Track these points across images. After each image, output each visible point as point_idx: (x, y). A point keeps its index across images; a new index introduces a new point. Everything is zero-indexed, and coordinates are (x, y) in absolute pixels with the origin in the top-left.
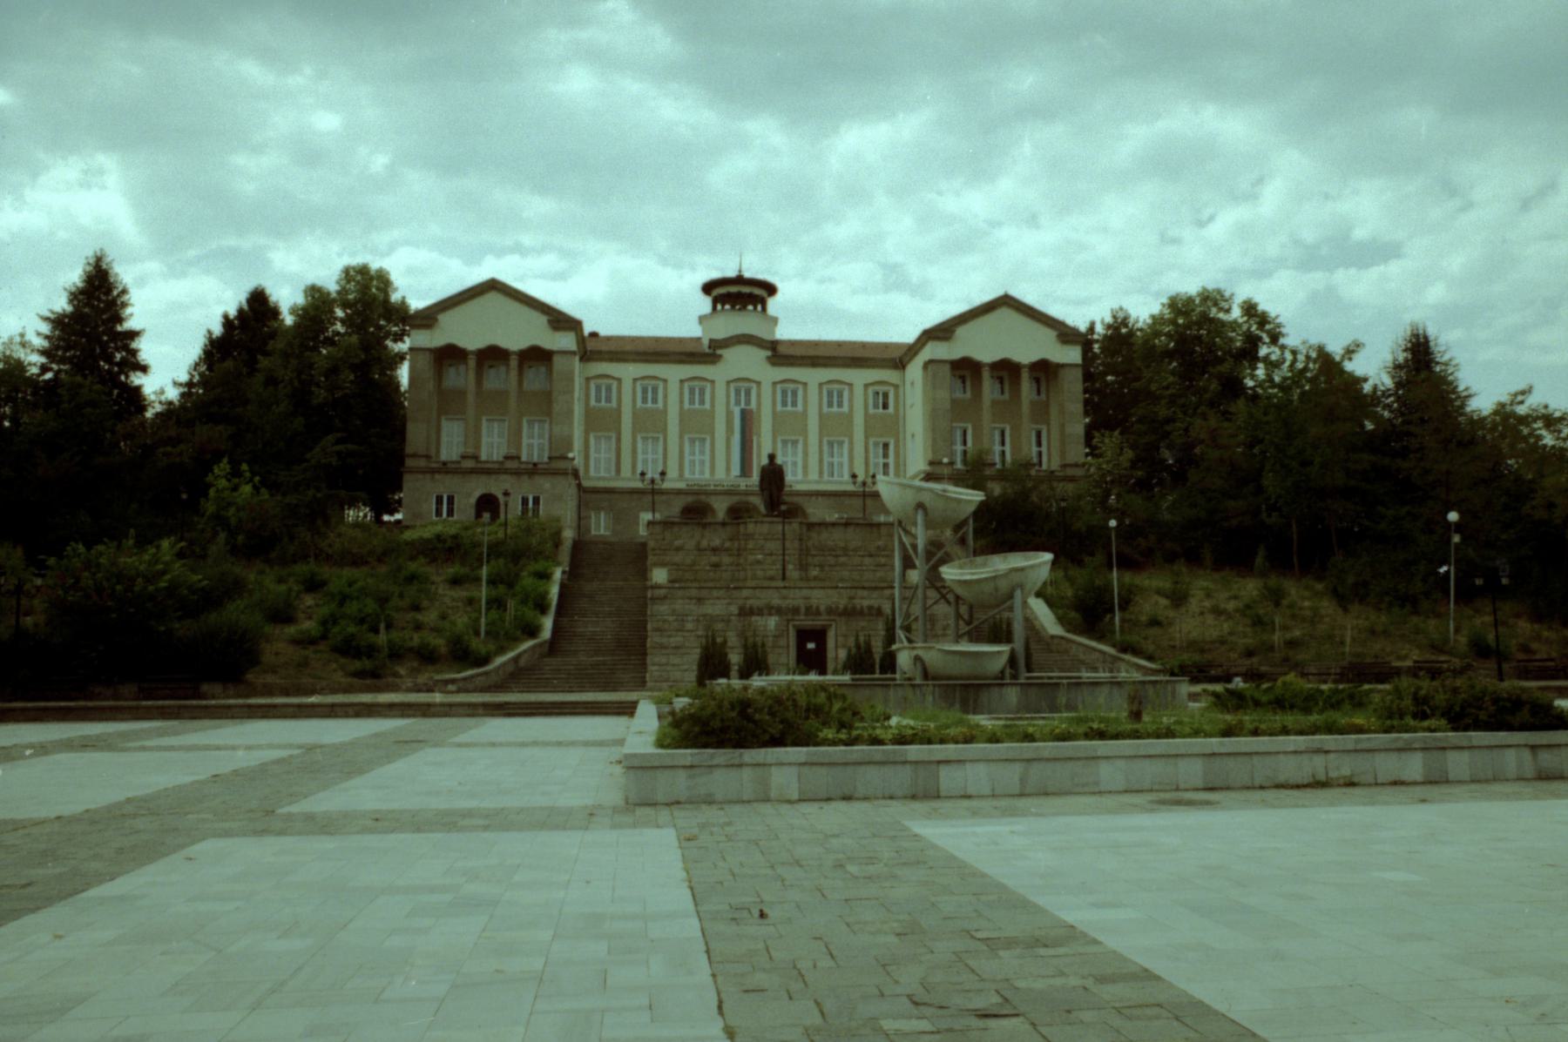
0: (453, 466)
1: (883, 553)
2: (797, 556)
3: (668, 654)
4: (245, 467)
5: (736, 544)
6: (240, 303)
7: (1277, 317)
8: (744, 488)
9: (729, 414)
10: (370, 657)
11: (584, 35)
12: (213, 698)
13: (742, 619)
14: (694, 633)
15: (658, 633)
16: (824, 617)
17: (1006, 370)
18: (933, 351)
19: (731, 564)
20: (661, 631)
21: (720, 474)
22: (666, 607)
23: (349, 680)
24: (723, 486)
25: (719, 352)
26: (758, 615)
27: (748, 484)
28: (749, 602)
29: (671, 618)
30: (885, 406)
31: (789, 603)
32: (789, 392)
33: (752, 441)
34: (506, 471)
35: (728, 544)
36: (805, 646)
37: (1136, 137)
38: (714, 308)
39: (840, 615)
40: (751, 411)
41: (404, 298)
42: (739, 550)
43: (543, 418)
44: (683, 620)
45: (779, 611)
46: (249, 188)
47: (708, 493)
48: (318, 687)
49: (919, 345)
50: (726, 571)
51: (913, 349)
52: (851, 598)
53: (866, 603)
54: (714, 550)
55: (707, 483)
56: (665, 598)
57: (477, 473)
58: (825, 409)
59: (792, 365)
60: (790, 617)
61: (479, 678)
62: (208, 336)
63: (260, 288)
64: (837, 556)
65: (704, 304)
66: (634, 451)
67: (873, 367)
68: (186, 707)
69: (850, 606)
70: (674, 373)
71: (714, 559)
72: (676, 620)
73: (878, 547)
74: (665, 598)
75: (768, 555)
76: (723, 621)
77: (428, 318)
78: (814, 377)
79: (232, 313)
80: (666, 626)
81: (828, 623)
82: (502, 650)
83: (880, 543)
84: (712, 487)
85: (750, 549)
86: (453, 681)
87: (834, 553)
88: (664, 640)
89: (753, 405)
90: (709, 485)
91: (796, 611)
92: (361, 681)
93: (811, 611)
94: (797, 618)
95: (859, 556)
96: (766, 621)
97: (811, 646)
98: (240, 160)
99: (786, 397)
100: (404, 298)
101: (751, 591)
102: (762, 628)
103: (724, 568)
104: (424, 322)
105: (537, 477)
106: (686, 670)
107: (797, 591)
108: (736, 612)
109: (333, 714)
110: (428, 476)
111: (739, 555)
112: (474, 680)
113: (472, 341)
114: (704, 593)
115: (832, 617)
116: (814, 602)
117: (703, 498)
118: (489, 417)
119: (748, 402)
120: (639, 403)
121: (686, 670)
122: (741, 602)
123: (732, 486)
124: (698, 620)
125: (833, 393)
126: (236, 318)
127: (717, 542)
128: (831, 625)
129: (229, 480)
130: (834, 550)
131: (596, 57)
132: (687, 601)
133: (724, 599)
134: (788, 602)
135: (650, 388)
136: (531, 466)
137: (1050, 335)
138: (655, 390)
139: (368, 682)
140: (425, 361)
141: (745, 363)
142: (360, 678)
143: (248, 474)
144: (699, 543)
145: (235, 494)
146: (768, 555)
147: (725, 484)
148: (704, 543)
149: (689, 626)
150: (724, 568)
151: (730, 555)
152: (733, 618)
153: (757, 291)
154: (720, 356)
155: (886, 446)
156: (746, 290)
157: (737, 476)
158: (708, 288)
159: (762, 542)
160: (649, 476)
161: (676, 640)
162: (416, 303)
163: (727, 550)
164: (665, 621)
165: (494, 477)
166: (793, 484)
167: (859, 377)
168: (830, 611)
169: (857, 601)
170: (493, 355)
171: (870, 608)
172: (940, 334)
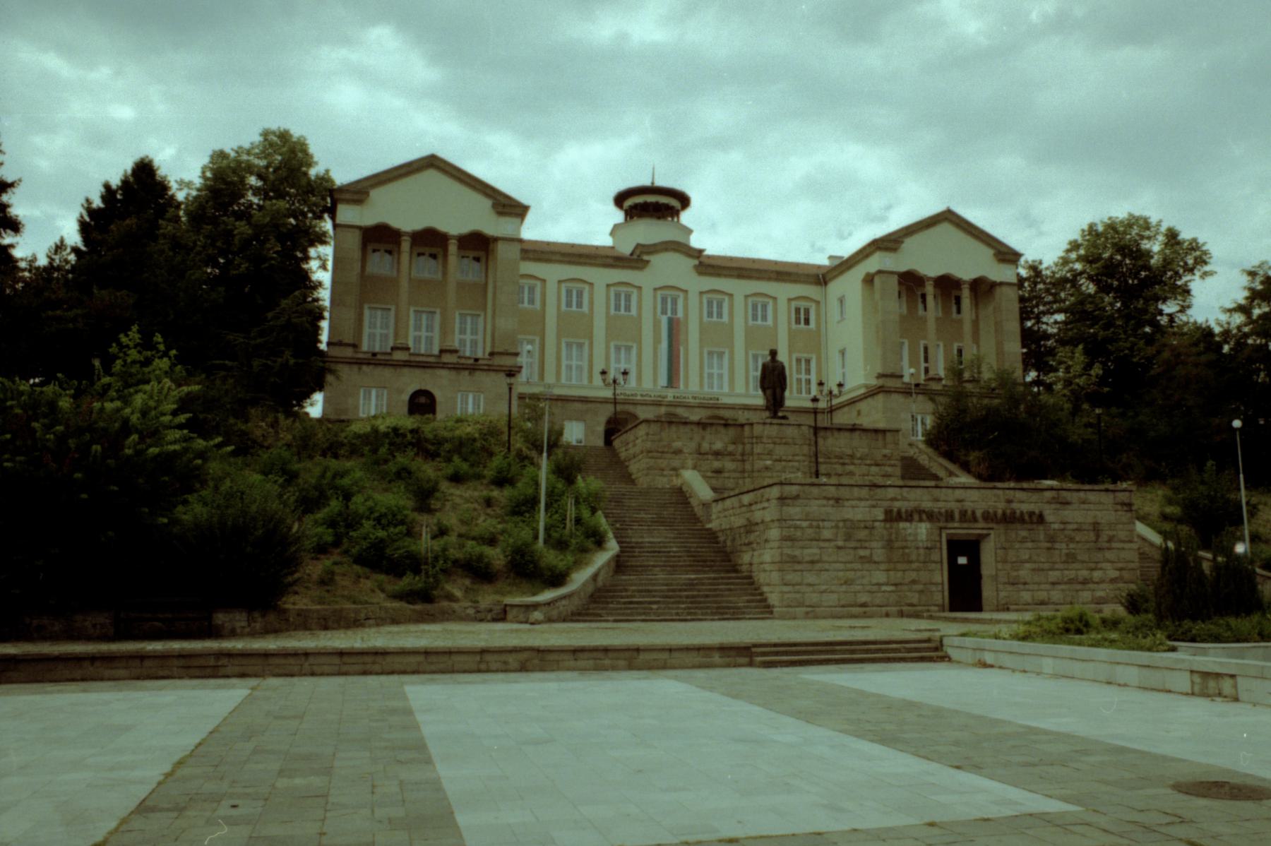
0: (383, 357)
1: (888, 462)
2: (806, 463)
3: (802, 571)
4: (158, 338)
5: (740, 448)
6: (125, 171)
7: (1204, 244)
8: (671, 399)
9: (656, 324)
10: (417, 571)
11: (354, 56)
12: (233, 634)
13: (888, 525)
14: (833, 544)
15: (789, 543)
16: (981, 524)
17: (947, 285)
18: (874, 263)
19: (734, 471)
20: (792, 540)
21: (647, 384)
22: (798, 509)
23: (396, 604)
24: (651, 396)
25: (646, 258)
26: (906, 520)
27: (677, 395)
28: (897, 504)
29: (805, 524)
30: (807, 322)
31: (942, 506)
32: (714, 301)
33: (679, 350)
34: (444, 366)
35: (731, 448)
36: (956, 560)
37: (800, 166)
38: (626, 219)
39: (998, 522)
40: (678, 320)
41: (327, 171)
42: (743, 454)
43: (478, 313)
44: (818, 527)
45: (930, 516)
46: (44, 164)
47: (635, 404)
48: (363, 616)
49: (861, 256)
50: (729, 478)
51: (843, 266)
52: (1009, 501)
53: (1026, 508)
54: (717, 454)
55: (633, 393)
56: (797, 497)
57: (410, 366)
58: (751, 322)
59: (719, 275)
60: (942, 524)
61: (564, 602)
62: (86, 205)
63: (147, 160)
64: (843, 464)
65: (618, 216)
66: (558, 359)
67: (795, 281)
68: (230, 655)
69: (1008, 512)
70: (600, 277)
71: (717, 464)
72: (811, 526)
73: (885, 456)
74: (797, 497)
75: (776, 460)
76: (866, 528)
77: (359, 192)
78: (739, 288)
79: (115, 182)
80: (799, 533)
81: (985, 532)
82: (578, 564)
83: (887, 451)
84: (639, 398)
85: (758, 454)
86: (535, 606)
87: (841, 461)
88: (797, 552)
89: (680, 314)
90: (636, 395)
91: (949, 516)
92: (411, 607)
93: (967, 517)
94: (950, 525)
95: (866, 465)
96: (916, 529)
97: (962, 560)
98: (39, 140)
99: (712, 307)
100: (327, 171)
101: (897, 490)
102: (911, 538)
103: (726, 475)
104: (356, 197)
105: (478, 373)
106: (824, 592)
107: (950, 491)
108: (881, 517)
109: (483, 666)
110: (355, 368)
111: (743, 461)
112: (557, 604)
113: (407, 220)
114: (844, 492)
115: (991, 525)
116: (968, 506)
117: (631, 408)
118: (416, 309)
119: (674, 311)
120: (563, 307)
121: (824, 592)
122: (886, 504)
123: (659, 396)
124: (837, 527)
125: (758, 307)
126: (120, 188)
127: (718, 446)
128: (988, 535)
129: (139, 352)
130: (842, 458)
131: (361, 74)
132: (824, 502)
133: (867, 500)
134: (941, 504)
135: (573, 292)
136: (471, 361)
137: (987, 253)
138: (580, 294)
139: (418, 607)
140: (354, 240)
141: (668, 269)
142: (409, 603)
143: (162, 347)
144: (700, 445)
145: (146, 370)
146: (776, 460)
147: (653, 395)
148: (705, 446)
149: (827, 534)
150: (726, 475)
151: (733, 461)
152: (877, 524)
153: (674, 203)
154: (648, 262)
155: (808, 361)
156: (663, 200)
157: (663, 387)
158: (620, 199)
159: (771, 446)
160: (611, 376)
161: (811, 552)
162: (342, 176)
163: (730, 454)
164: (796, 527)
165: (429, 371)
166: (720, 398)
167: (784, 291)
168: (987, 517)
169: (1015, 506)
170: (430, 241)
171: (1031, 514)
172: (890, 245)
